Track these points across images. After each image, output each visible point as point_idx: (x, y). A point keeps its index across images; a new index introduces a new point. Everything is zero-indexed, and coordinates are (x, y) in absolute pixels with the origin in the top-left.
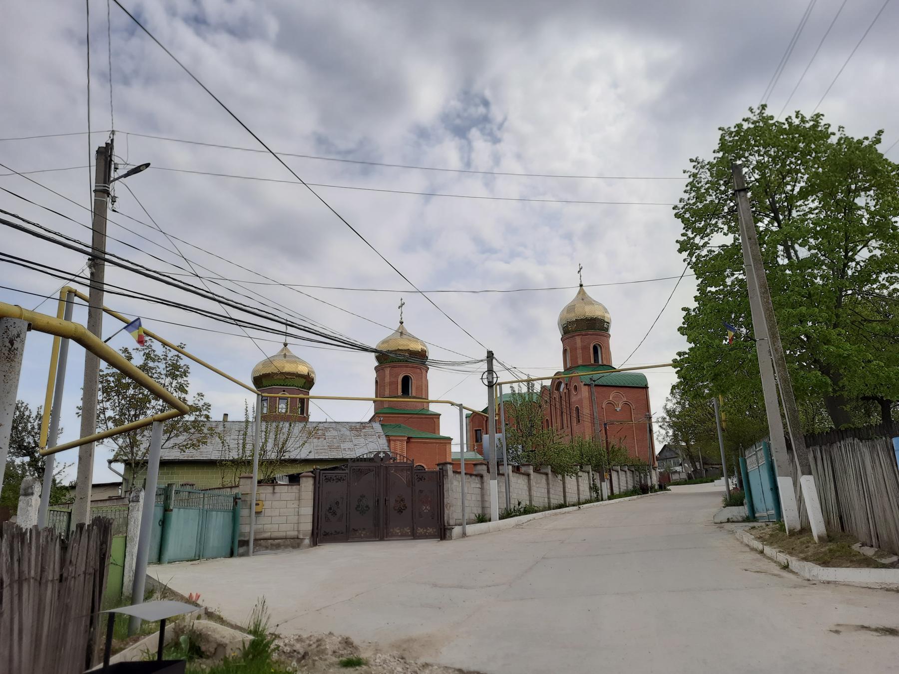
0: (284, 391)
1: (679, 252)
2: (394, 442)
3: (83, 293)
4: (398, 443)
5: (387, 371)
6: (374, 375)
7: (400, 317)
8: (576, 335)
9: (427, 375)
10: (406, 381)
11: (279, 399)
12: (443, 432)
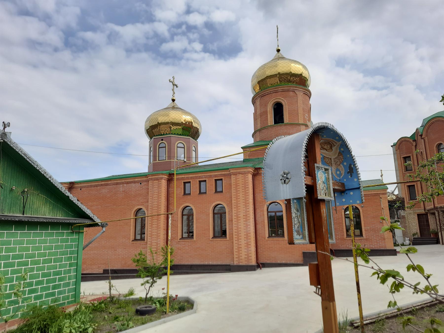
0: (162, 140)
2: (234, 176)
3: (394, 168)
6: (252, 109)
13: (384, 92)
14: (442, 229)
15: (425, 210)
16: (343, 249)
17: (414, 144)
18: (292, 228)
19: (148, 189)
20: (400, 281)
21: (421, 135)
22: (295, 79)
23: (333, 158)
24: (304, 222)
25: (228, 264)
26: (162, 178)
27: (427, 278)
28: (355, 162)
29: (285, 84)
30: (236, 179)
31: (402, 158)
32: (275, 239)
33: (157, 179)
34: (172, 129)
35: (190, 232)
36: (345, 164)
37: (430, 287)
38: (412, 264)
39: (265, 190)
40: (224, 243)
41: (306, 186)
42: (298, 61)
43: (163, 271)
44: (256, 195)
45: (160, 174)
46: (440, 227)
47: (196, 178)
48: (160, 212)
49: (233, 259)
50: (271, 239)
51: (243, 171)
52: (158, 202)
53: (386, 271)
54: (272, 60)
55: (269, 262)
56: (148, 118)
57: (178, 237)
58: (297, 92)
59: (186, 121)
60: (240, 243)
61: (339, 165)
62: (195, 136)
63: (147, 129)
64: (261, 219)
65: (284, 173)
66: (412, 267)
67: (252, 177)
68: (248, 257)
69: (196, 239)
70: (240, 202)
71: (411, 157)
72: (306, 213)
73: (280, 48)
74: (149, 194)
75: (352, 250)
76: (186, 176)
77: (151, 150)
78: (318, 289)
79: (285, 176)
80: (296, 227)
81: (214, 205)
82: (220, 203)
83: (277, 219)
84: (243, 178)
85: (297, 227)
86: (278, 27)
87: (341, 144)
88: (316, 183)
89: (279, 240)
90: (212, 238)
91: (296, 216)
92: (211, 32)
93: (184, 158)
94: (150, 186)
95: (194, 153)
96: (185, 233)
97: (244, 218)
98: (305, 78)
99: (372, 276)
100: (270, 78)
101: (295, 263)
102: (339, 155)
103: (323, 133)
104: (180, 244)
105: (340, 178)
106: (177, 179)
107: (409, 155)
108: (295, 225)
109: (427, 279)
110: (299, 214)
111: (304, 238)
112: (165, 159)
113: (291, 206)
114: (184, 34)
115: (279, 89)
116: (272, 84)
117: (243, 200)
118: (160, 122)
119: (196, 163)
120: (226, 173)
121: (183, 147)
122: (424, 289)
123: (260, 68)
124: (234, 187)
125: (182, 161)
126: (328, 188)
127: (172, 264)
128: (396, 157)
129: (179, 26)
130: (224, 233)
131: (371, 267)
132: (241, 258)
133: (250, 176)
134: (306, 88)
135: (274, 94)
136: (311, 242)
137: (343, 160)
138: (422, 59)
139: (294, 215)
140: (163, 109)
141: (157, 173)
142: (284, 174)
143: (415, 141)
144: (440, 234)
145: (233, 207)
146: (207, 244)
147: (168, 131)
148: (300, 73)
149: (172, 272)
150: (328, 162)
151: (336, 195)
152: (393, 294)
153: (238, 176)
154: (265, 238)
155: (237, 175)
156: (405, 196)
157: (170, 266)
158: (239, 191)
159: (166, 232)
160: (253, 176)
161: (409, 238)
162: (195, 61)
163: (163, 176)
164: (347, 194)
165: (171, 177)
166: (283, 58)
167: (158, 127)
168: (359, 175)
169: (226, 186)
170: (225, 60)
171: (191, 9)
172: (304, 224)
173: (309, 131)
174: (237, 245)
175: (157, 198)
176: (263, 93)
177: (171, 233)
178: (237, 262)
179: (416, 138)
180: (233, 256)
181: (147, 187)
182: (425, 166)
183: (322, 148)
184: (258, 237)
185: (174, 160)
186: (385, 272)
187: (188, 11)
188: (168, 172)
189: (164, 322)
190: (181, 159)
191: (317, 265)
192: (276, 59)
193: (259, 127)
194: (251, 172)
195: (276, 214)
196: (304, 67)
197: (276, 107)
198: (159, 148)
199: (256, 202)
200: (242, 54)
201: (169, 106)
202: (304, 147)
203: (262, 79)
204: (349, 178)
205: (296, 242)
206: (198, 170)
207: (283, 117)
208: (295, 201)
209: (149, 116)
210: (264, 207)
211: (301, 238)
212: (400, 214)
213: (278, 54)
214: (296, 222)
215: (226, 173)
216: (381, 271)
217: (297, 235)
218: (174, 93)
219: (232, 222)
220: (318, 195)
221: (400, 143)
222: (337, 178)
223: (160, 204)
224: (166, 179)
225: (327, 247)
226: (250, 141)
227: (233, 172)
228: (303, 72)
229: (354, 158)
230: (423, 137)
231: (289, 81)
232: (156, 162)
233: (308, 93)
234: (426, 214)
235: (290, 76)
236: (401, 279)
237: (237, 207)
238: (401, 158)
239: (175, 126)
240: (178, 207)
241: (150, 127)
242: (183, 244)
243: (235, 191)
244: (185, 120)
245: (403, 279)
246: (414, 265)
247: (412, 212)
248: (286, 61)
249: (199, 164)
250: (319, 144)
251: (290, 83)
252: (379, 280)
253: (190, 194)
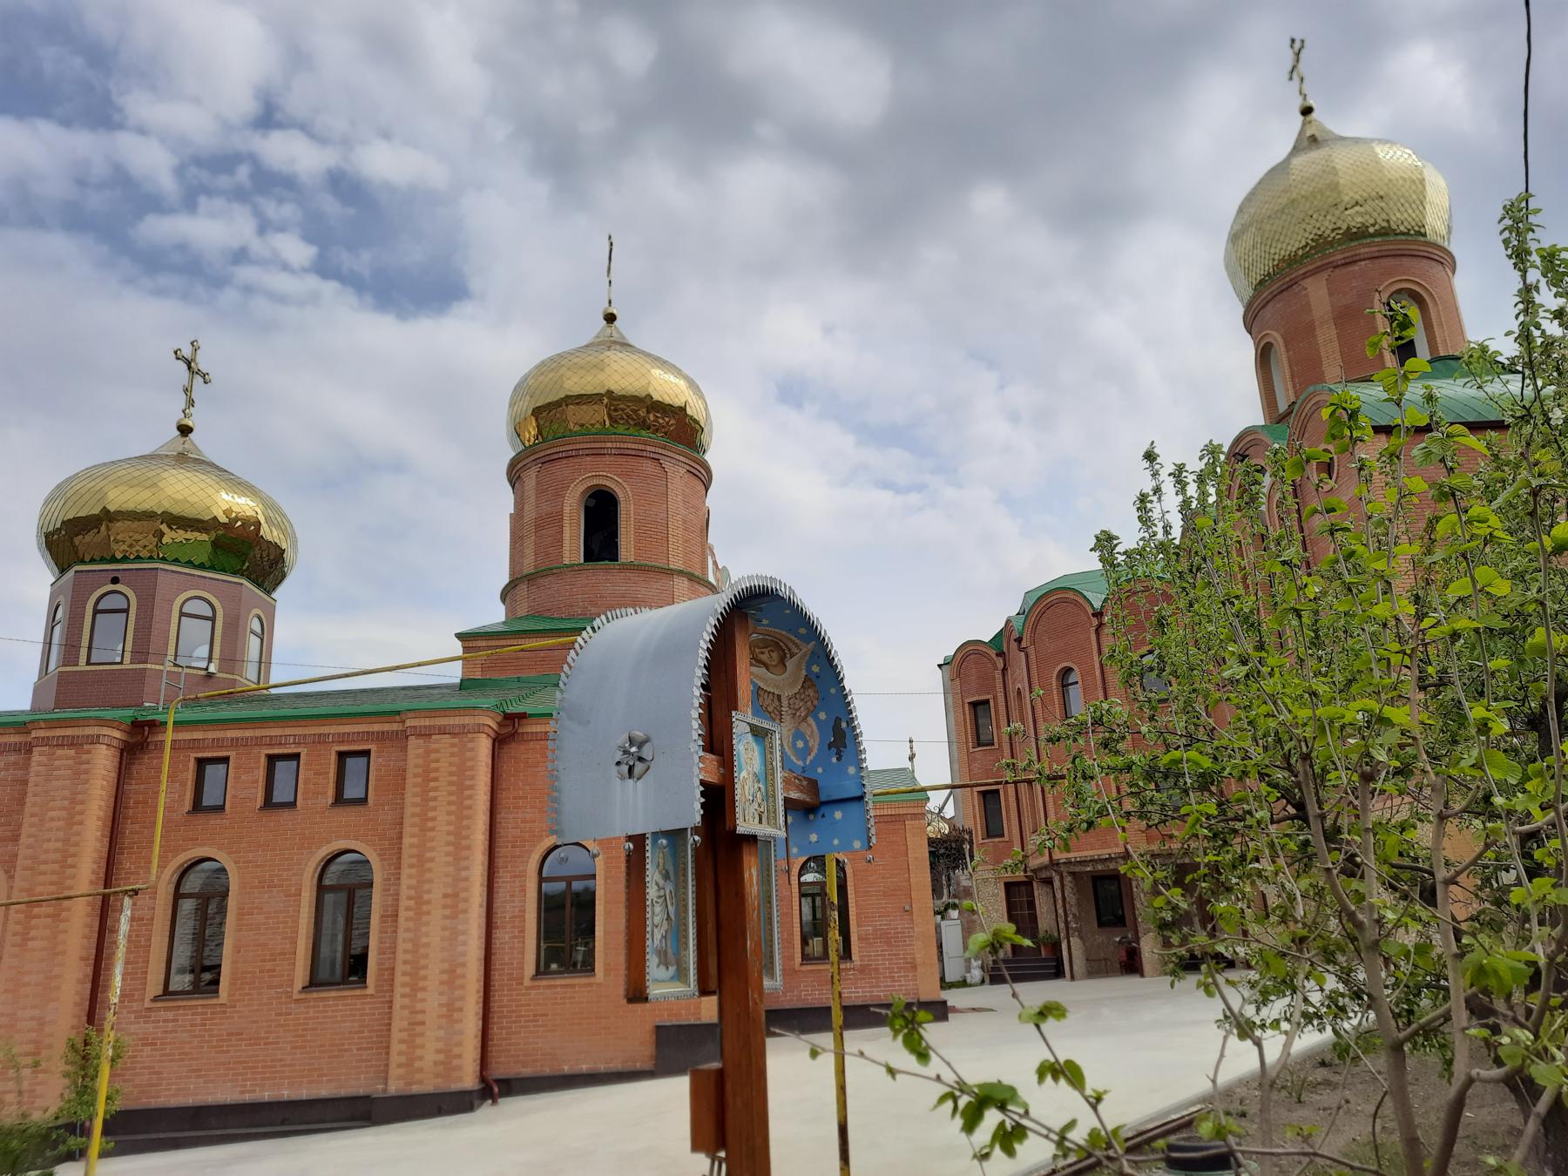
0: (115, 581)
3: (943, 735)
6: (505, 500)
8: (1305, 276)
13: (914, 498)
14: (1071, 932)
15: (1025, 871)
16: (788, 1007)
17: (1000, 663)
18: (644, 940)
19: (25, 782)
20: (1016, 1118)
21: (1019, 640)
22: (661, 421)
23: (786, 693)
24: (686, 918)
25: (361, 1092)
26: (95, 740)
27: (1095, 1102)
28: (851, 712)
29: (626, 432)
30: (428, 752)
31: (967, 706)
32: (558, 982)
33: (73, 743)
34: (164, 540)
35: (205, 969)
36: (822, 716)
37: (1103, 1133)
38: (1053, 1060)
39: (555, 800)
40: (352, 1010)
41: (702, 789)
42: (680, 367)
43: (64, 1142)
44: (501, 816)
45: (92, 722)
46: (1067, 923)
47: (258, 742)
48: (69, 882)
49: (387, 1072)
50: (544, 983)
51: (459, 726)
52: (66, 841)
53: (980, 1086)
54: (587, 346)
55: (527, 1071)
56: (58, 486)
57: (145, 989)
58: (667, 465)
59: (234, 515)
60: (419, 1006)
61: (805, 719)
62: (265, 575)
63: (51, 529)
64: (513, 907)
65: (631, 741)
66: (1055, 1070)
67: (491, 747)
68: (448, 1062)
69: (229, 995)
70: (434, 844)
71: (992, 704)
72: (694, 883)
73: (615, 312)
74: (28, 804)
75: (830, 1008)
76: (211, 735)
77: (57, 619)
78: (716, 1164)
79: (634, 749)
80: (658, 936)
81: (324, 854)
82: (352, 848)
83: (572, 905)
84: (455, 750)
85: (659, 937)
86: (613, 239)
87: (813, 653)
88: (732, 778)
89: (573, 986)
90: (303, 988)
91: (660, 897)
92: (351, 211)
93: (210, 660)
94: (34, 768)
95: (254, 642)
96: (181, 971)
97: (445, 907)
98: (697, 422)
99: (936, 1107)
100: (578, 404)
101: (626, 1070)
102: (806, 685)
103: (761, 610)
104: (154, 1022)
105: (805, 763)
106: (176, 745)
108: (656, 930)
109: (1094, 1108)
110: (669, 887)
111: (681, 975)
112: (118, 659)
113: (644, 858)
114: (240, 195)
115: (609, 445)
116: (582, 425)
118: (112, 508)
119: (262, 685)
120: (386, 727)
121: (211, 615)
122: (1086, 1140)
123: (543, 363)
124: (416, 785)
125: (195, 672)
126: (769, 796)
127: (114, 1108)
128: (950, 701)
129: (223, 162)
130: (356, 967)
131: (934, 1076)
132: (418, 1064)
133: (484, 746)
134: (696, 455)
136: (704, 991)
137: (816, 702)
138: (1014, 418)
139: (652, 892)
140: (122, 458)
141: (77, 715)
142: (631, 744)
143: (1001, 654)
144: (1064, 946)
145: (406, 861)
146: (277, 1015)
147: (145, 546)
148: (678, 402)
149: (107, 1143)
150: (770, 709)
151: (790, 820)
152: (985, 1164)
154: (522, 978)
155: (433, 737)
156: (973, 821)
157: (105, 1122)
158: (435, 799)
159: (90, 970)
160: (497, 744)
161: (980, 962)
162: (281, 299)
163: (105, 731)
164: (823, 816)
165: (139, 737)
166: (625, 345)
167: (103, 528)
168: (863, 756)
169: (380, 780)
170: (402, 315)
171: (279, 116)
172: (686, 925)
173: (719, 603)
174: (406, 1012)
175: (61, 824)
176: (549, 452)
177: (123, 980)
178: (401, 1084)
179: (1005, 646)
180: (388, 1059)
181: (21, 772)
182: (1058, 740)
183: (756, 661)
184: (496, 976)
185: (161, 667)
186: (976, 1090)
187: (268, 118)
188: (129, 713)
190: (193, 665)
191: (720, 1074)
192: (600, 344)
193: (528, 566)
194: (487, 730)
195: (569, 885)
196: (692, 384)
197: (592, 503)
198: (96, 612)
199: (500, 842)
200: (467, 308)
201: (164, 448)
202: (703, 654)
203: (547, 401)
204: (830, 763)
205: (654, 991)
206: (266, 712)
207: (617, 543)
208: (664, 842)
209: (67, 480)
210: (527, 862)
211: (672, 978)
212: (958, 884)
213: (609, 331)
214: (657, 920)
215: (386, 727)
216: (962, 1087)
217: (658, 966)
218: (191, 403)
219: (396, 921)
220: (738, 822)
221: (964, 659)
222: (795, 760)
223: (72, 850)
224: (115, 743)
225: (756, 1003)
226: (494, 614)
227: (415, 727)
228: (690, 401)
229: (850, 698)
230: (1024, 644)
231: (643, 425)
232: (75, 669)
233: (703, 471)
234: (1028, 884)
235: (647, 407)
236: (1021, 1111)
237: (422, 862)
238: (963, 702)
239: (181, 532)
240: (162, 867)
241: (63, 522)
242: (165, 1021)
243: (418, 800)
244: (227, 512)
245: (1027, 1112)
246: (1057, 1060)
247: (991, 876)
248: (635, 357)
249: (273, 691)
250: (747, 646)
251: (644, 433)
252: (959, 1121)
253: (220, 809)
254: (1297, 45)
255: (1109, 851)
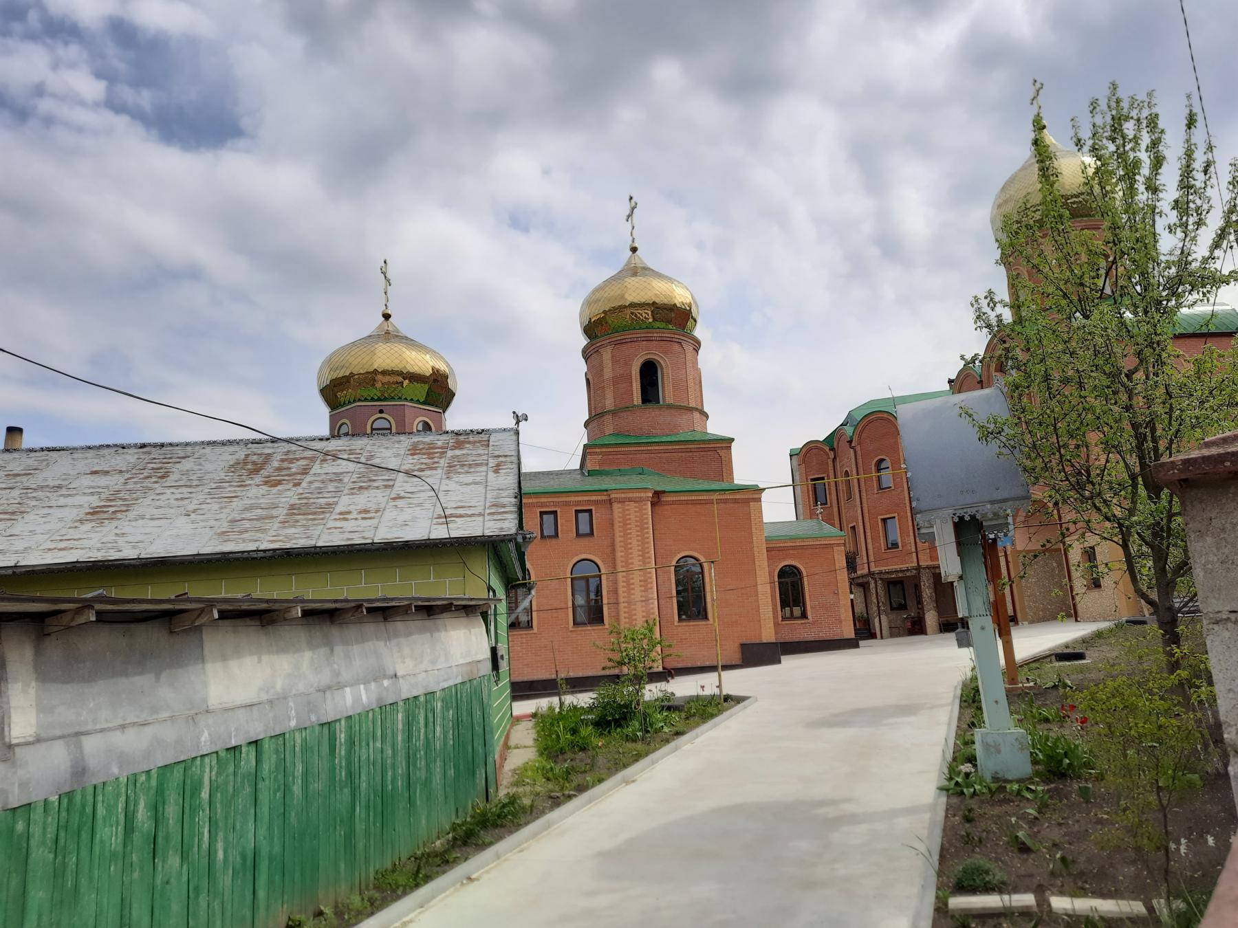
0: (381, 412)
1: (691, 618)
2: (620, 505)
4: (631, 506)
5: (607, 354)
6: (583, 367)
7: (631, 238)
9: (697, 359)
10: (649, 372)
11: (390, 429)
12: (742, 475)
17: (832, 455)
21: (850, 442)
30: (624, 511)
46: (878, 607)
73: (637, 245)
107: (822, 476)
115: (655, 335)
117: (639, 551)
120: (599, 498)
135: (644, 343)
138: (700, 246)
143: (832, 449)
153: (628, 505)
162: (80, 130)
176: (619, 338)
189: (715, 726)
200: (242, 143)
221: (807, 452)
230: (853, 445)
238: (807, 479)
254: (1038, 85)
255: (907, 565)
